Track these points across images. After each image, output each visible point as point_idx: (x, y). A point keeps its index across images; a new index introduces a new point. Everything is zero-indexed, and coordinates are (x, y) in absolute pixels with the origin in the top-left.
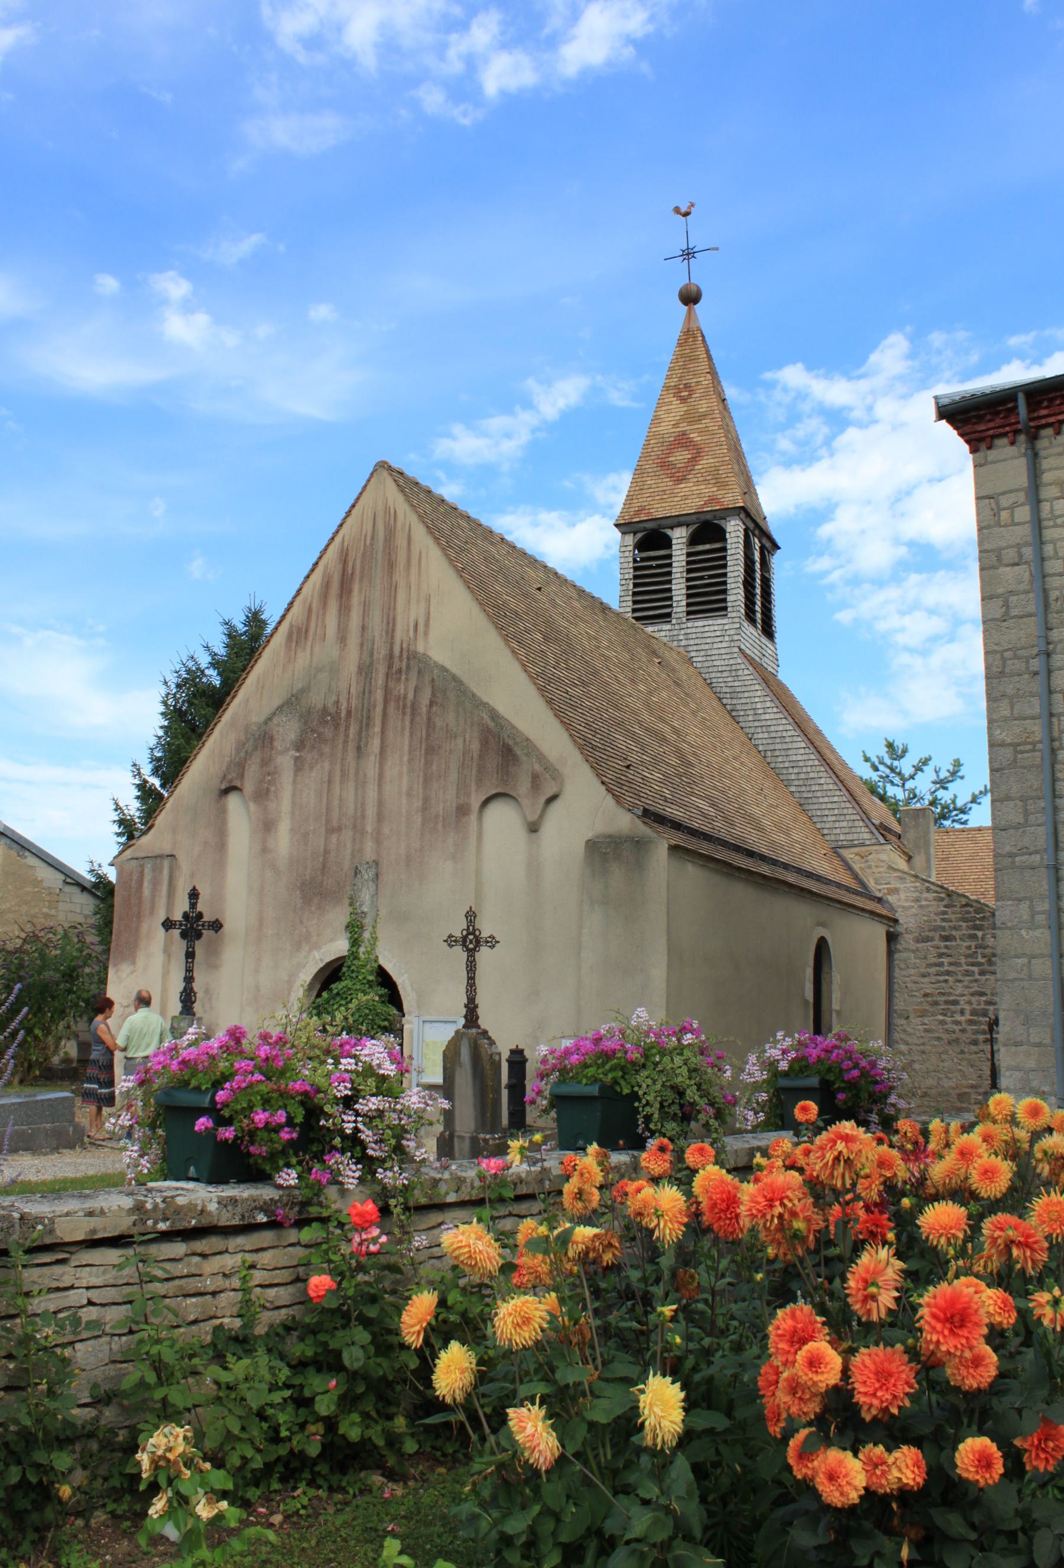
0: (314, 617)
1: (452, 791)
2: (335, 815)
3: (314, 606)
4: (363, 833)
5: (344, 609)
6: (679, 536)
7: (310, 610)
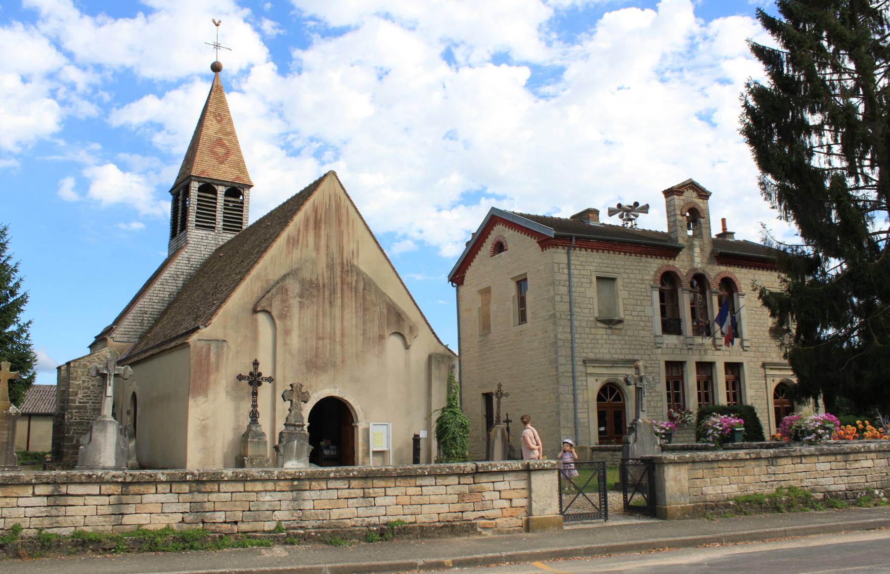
0: (301, 235)
1: (376, 329)
2: (321, 331)
3: (301, 229)
4: (335, 341)
5: (317, 235)
6: (221, 190)
7: (299, 231)
